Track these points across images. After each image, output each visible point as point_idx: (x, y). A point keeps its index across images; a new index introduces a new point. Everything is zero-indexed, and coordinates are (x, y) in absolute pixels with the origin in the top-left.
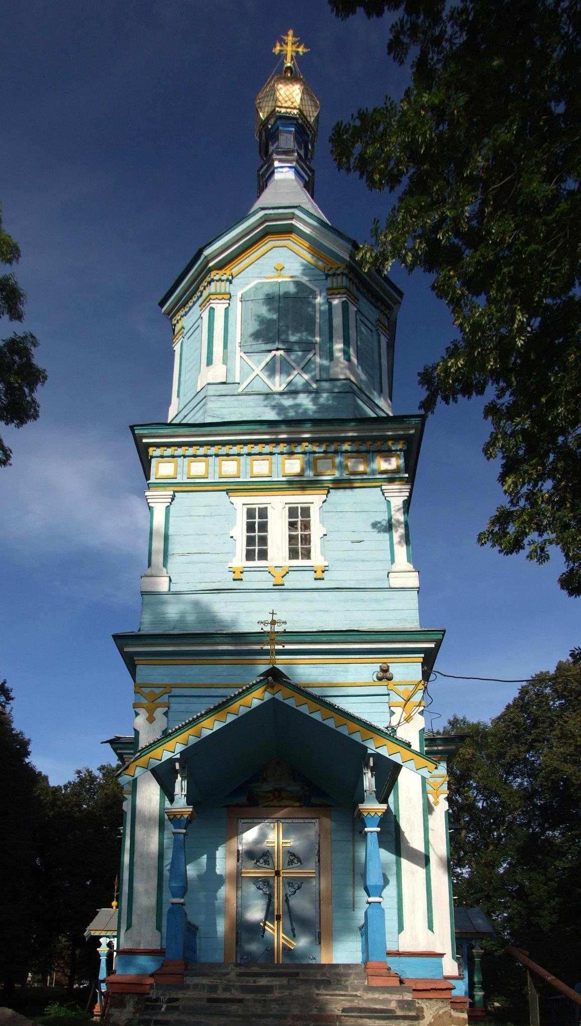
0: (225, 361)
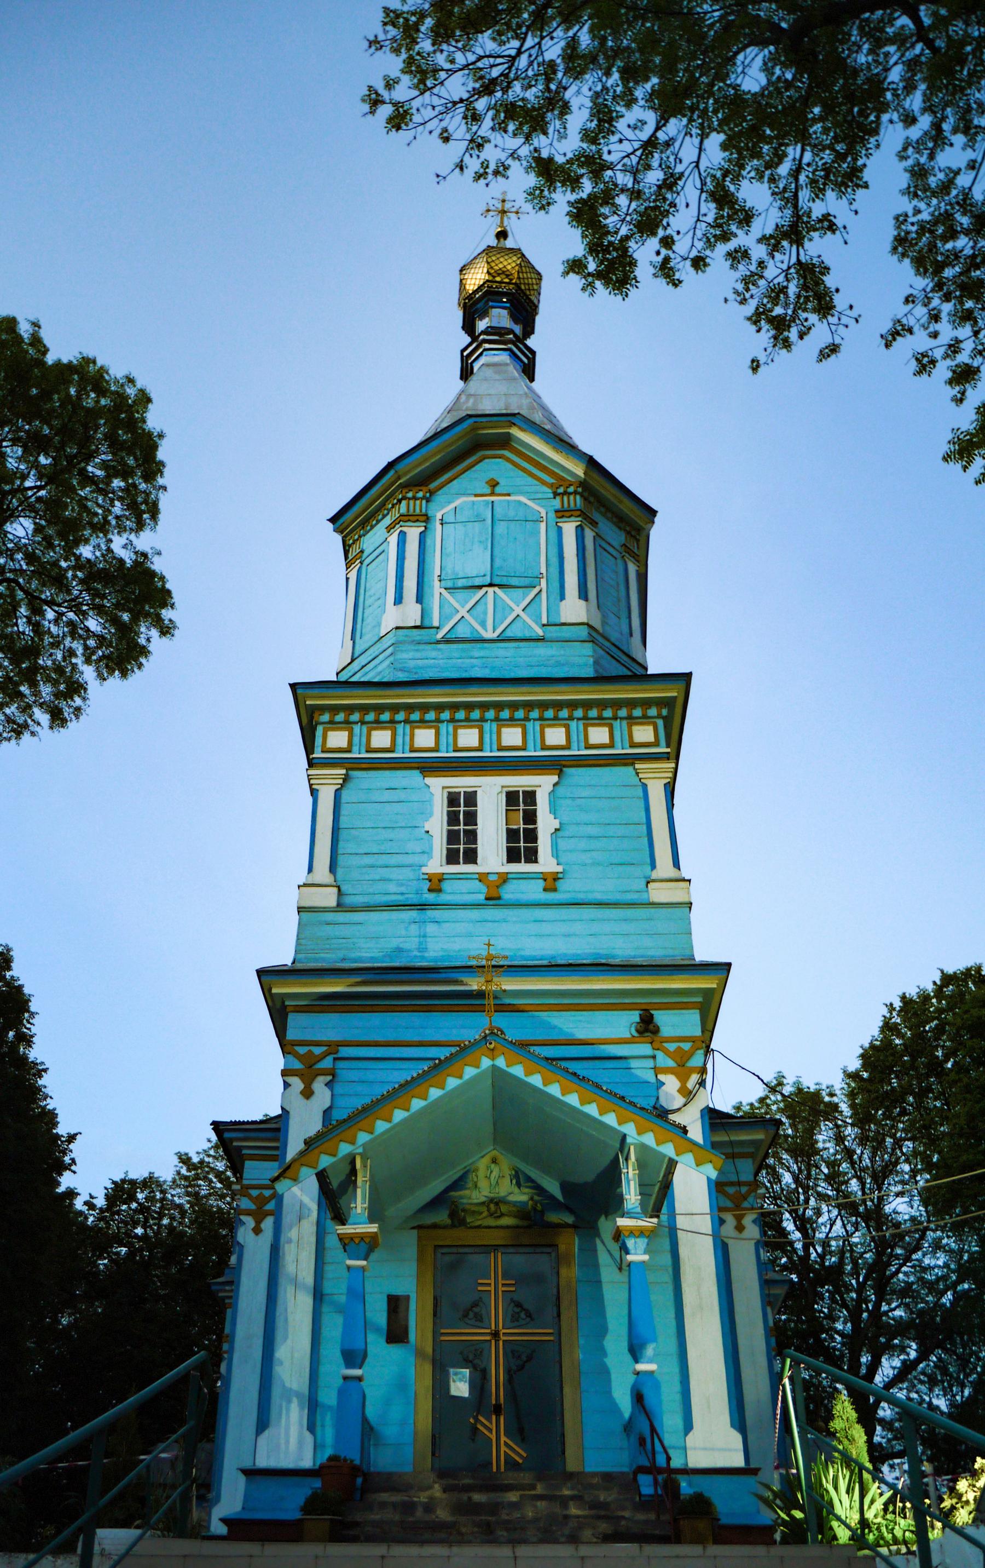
0: (419, 599)
